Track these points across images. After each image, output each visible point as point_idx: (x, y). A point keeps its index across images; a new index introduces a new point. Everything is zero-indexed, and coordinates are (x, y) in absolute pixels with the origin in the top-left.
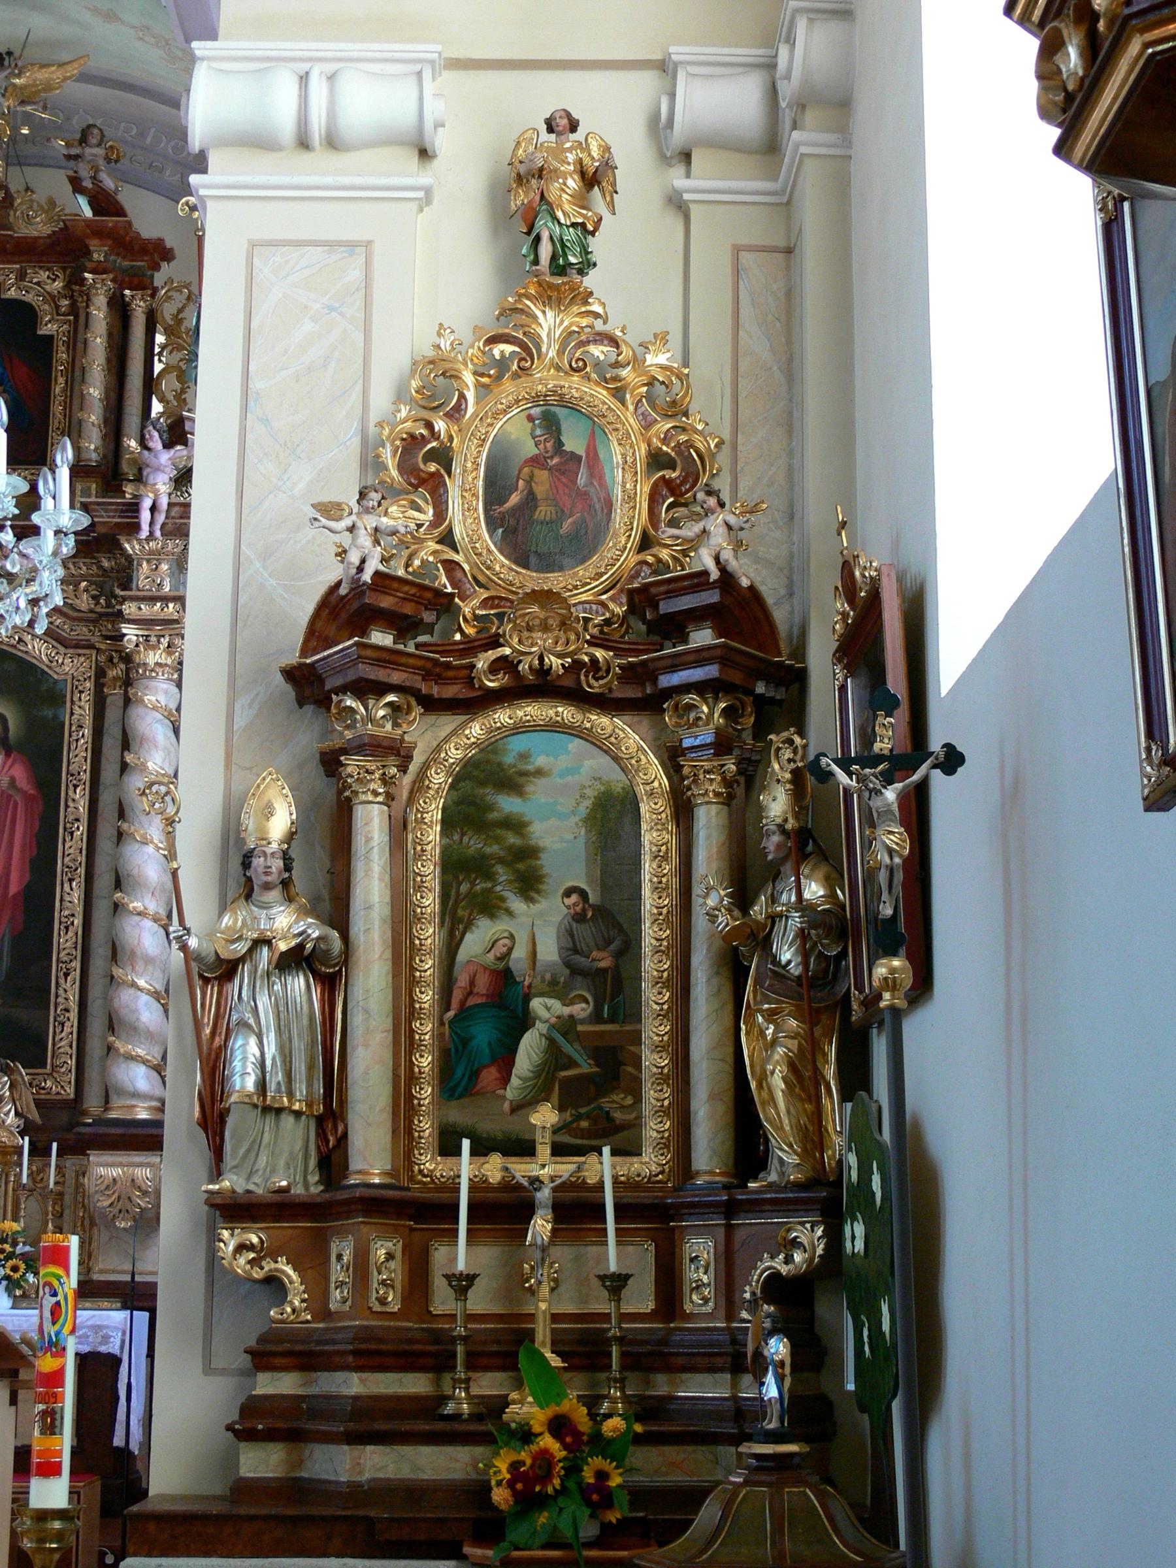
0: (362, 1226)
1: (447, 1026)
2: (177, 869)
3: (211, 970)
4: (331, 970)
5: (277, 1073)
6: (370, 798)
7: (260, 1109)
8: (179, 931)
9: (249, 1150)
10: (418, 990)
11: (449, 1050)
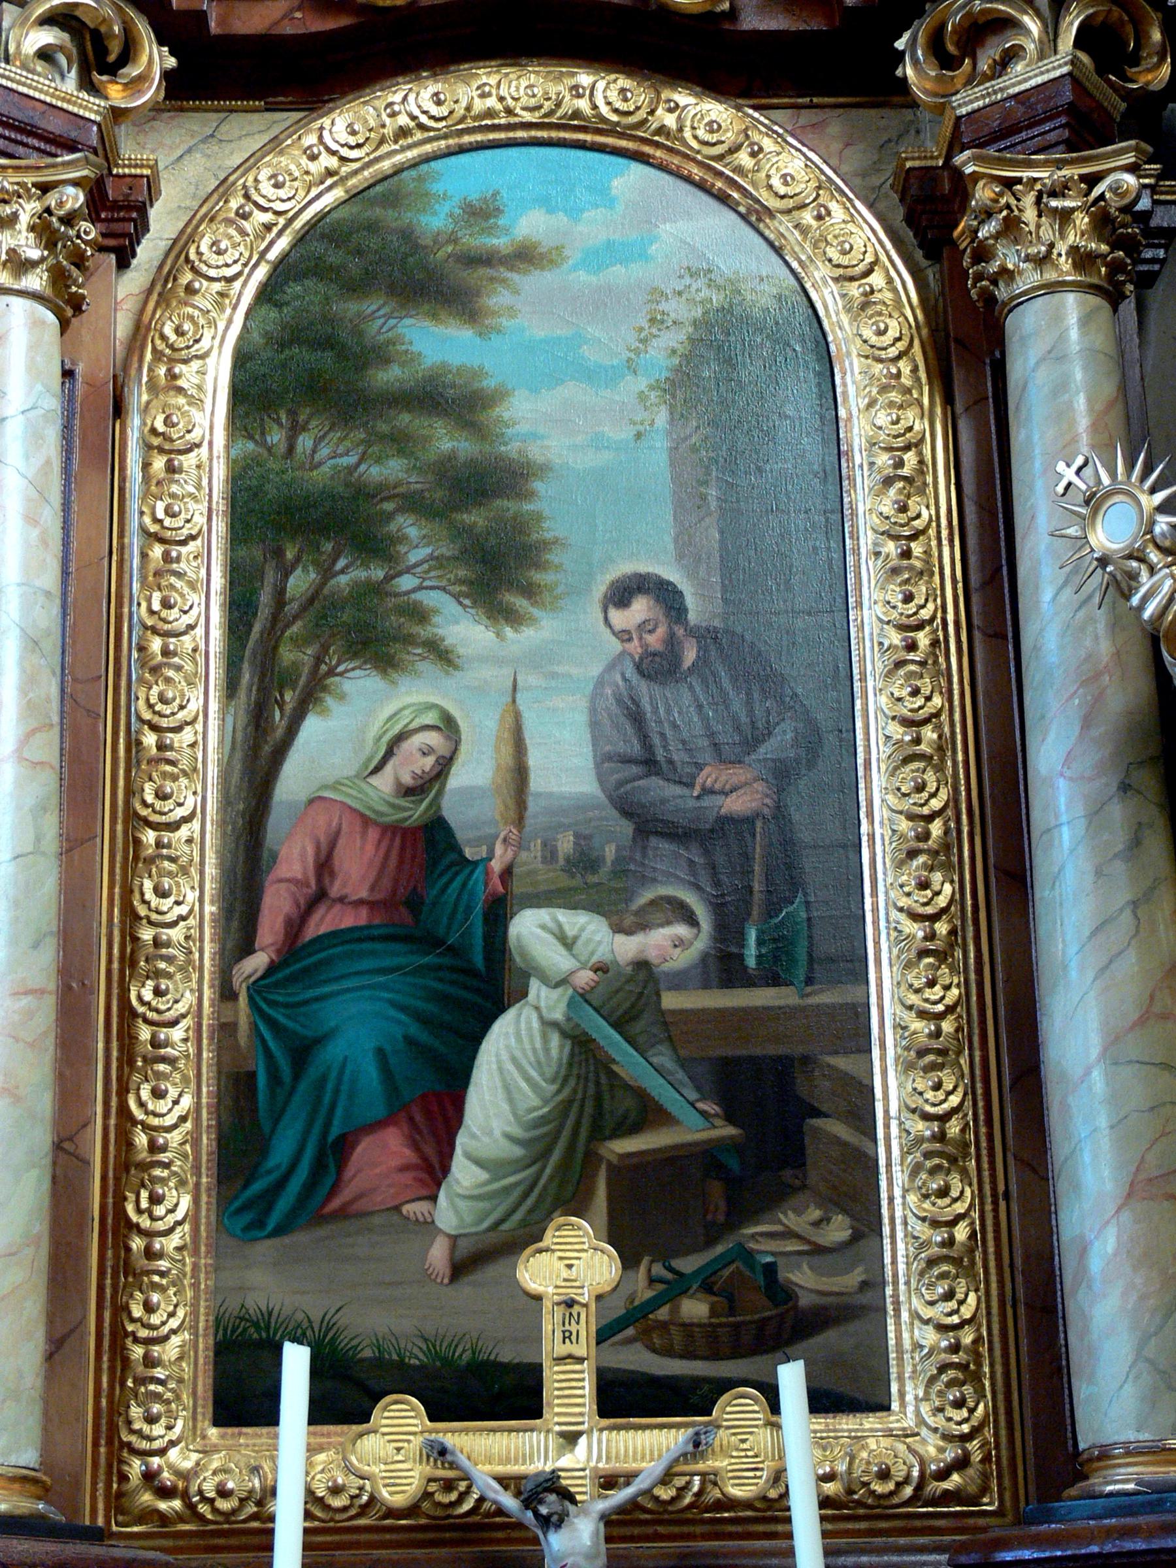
1: (243, 999)
10: (148, 885)
11: (252, 1075)
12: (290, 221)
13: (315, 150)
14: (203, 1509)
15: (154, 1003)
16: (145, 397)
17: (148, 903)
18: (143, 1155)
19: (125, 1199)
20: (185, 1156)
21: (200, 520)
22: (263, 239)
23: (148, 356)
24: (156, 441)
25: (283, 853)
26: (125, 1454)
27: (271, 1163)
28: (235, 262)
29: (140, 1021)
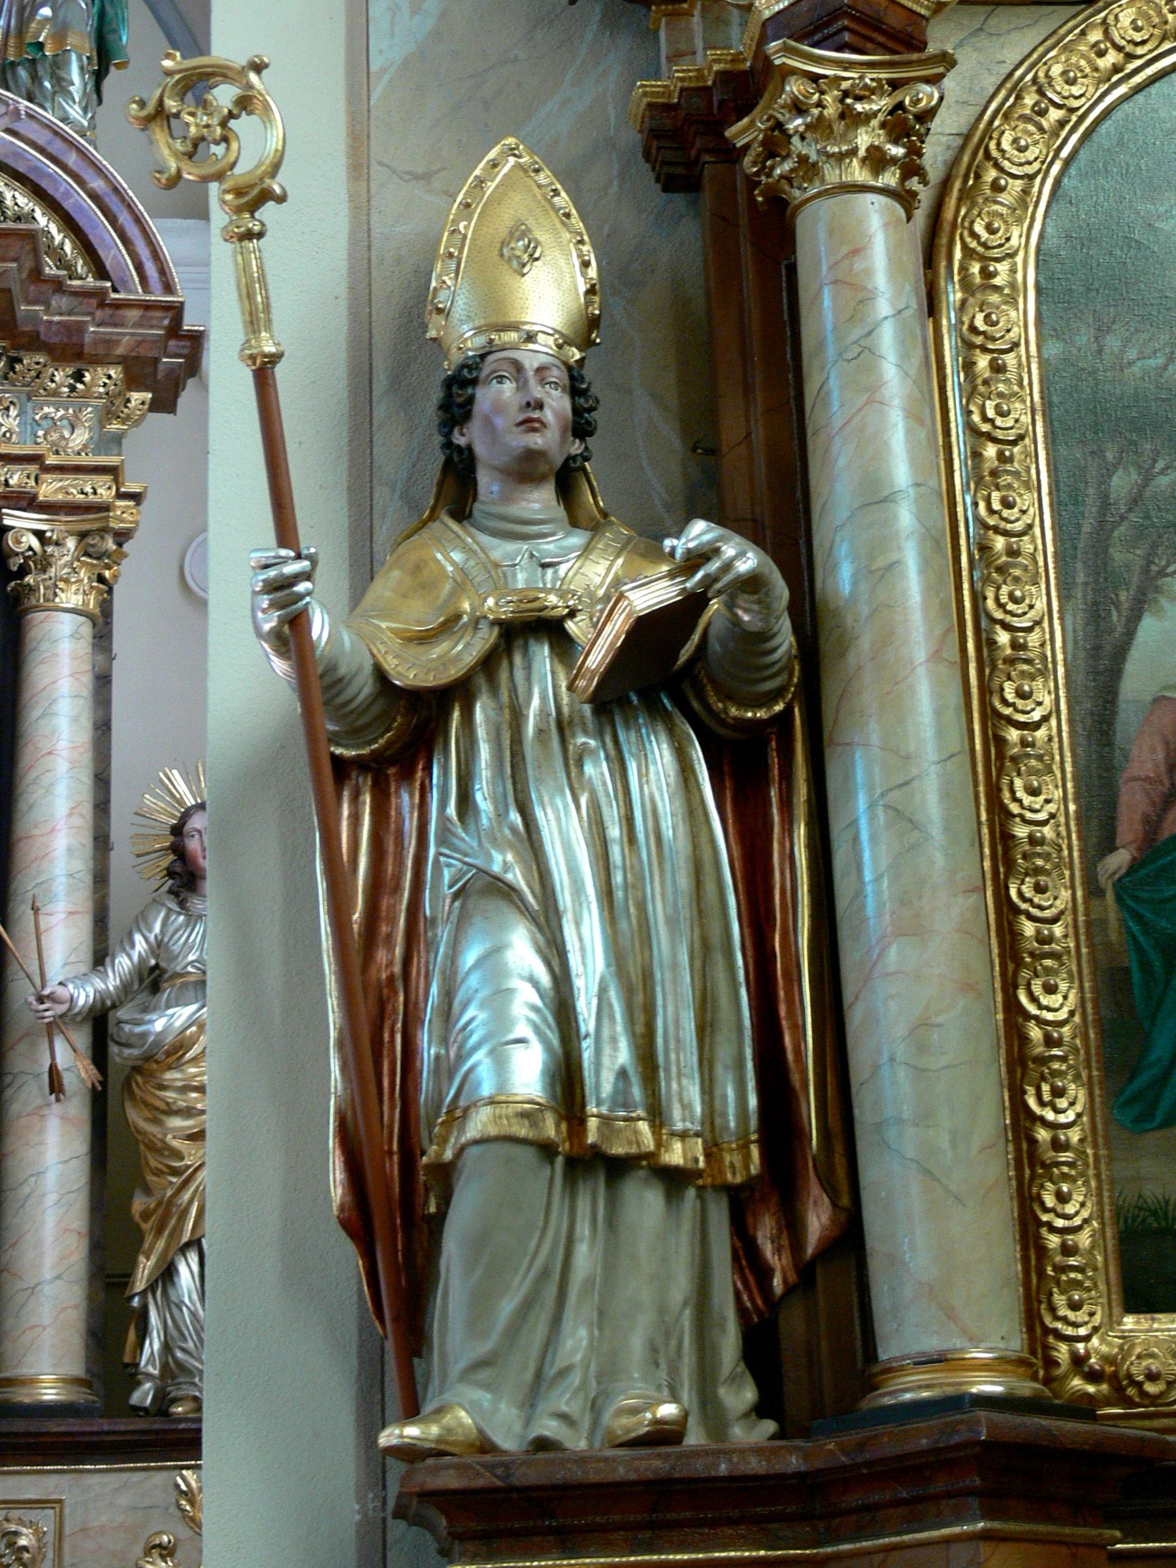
0: (985, 1549)
1: (1110, 897)
2: (275, 358)
3: (353, 734)
4: (761, 714)
5: (614, 1040)
6: (858, 173)
7: (560, 1160)
8: (285, 561)
9: (527, 1305)
10: (1018, 783)
11: (1126, 971)
12: (1081, 119)
13: (1102, 46)
14: (1131, 1391)
15: (1036, 900)
16: (959, 295)
17: (1020, 801)
18: (1040, 1050)
19: (1024, 1092)
20: (1076, 1050)
21: (1026, 419)
22: (1058, 136)
23: (958, 254)
24: (979, 340)
25: (1135, 752)
26: (1051, 1339)
27: (1153, 1057)
28: (1036, 159)
29: (1023, 917)
